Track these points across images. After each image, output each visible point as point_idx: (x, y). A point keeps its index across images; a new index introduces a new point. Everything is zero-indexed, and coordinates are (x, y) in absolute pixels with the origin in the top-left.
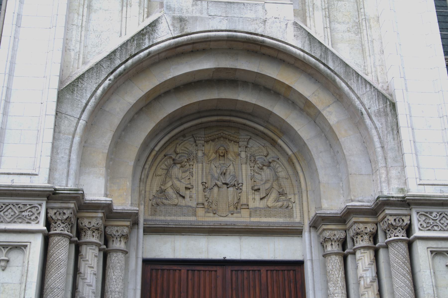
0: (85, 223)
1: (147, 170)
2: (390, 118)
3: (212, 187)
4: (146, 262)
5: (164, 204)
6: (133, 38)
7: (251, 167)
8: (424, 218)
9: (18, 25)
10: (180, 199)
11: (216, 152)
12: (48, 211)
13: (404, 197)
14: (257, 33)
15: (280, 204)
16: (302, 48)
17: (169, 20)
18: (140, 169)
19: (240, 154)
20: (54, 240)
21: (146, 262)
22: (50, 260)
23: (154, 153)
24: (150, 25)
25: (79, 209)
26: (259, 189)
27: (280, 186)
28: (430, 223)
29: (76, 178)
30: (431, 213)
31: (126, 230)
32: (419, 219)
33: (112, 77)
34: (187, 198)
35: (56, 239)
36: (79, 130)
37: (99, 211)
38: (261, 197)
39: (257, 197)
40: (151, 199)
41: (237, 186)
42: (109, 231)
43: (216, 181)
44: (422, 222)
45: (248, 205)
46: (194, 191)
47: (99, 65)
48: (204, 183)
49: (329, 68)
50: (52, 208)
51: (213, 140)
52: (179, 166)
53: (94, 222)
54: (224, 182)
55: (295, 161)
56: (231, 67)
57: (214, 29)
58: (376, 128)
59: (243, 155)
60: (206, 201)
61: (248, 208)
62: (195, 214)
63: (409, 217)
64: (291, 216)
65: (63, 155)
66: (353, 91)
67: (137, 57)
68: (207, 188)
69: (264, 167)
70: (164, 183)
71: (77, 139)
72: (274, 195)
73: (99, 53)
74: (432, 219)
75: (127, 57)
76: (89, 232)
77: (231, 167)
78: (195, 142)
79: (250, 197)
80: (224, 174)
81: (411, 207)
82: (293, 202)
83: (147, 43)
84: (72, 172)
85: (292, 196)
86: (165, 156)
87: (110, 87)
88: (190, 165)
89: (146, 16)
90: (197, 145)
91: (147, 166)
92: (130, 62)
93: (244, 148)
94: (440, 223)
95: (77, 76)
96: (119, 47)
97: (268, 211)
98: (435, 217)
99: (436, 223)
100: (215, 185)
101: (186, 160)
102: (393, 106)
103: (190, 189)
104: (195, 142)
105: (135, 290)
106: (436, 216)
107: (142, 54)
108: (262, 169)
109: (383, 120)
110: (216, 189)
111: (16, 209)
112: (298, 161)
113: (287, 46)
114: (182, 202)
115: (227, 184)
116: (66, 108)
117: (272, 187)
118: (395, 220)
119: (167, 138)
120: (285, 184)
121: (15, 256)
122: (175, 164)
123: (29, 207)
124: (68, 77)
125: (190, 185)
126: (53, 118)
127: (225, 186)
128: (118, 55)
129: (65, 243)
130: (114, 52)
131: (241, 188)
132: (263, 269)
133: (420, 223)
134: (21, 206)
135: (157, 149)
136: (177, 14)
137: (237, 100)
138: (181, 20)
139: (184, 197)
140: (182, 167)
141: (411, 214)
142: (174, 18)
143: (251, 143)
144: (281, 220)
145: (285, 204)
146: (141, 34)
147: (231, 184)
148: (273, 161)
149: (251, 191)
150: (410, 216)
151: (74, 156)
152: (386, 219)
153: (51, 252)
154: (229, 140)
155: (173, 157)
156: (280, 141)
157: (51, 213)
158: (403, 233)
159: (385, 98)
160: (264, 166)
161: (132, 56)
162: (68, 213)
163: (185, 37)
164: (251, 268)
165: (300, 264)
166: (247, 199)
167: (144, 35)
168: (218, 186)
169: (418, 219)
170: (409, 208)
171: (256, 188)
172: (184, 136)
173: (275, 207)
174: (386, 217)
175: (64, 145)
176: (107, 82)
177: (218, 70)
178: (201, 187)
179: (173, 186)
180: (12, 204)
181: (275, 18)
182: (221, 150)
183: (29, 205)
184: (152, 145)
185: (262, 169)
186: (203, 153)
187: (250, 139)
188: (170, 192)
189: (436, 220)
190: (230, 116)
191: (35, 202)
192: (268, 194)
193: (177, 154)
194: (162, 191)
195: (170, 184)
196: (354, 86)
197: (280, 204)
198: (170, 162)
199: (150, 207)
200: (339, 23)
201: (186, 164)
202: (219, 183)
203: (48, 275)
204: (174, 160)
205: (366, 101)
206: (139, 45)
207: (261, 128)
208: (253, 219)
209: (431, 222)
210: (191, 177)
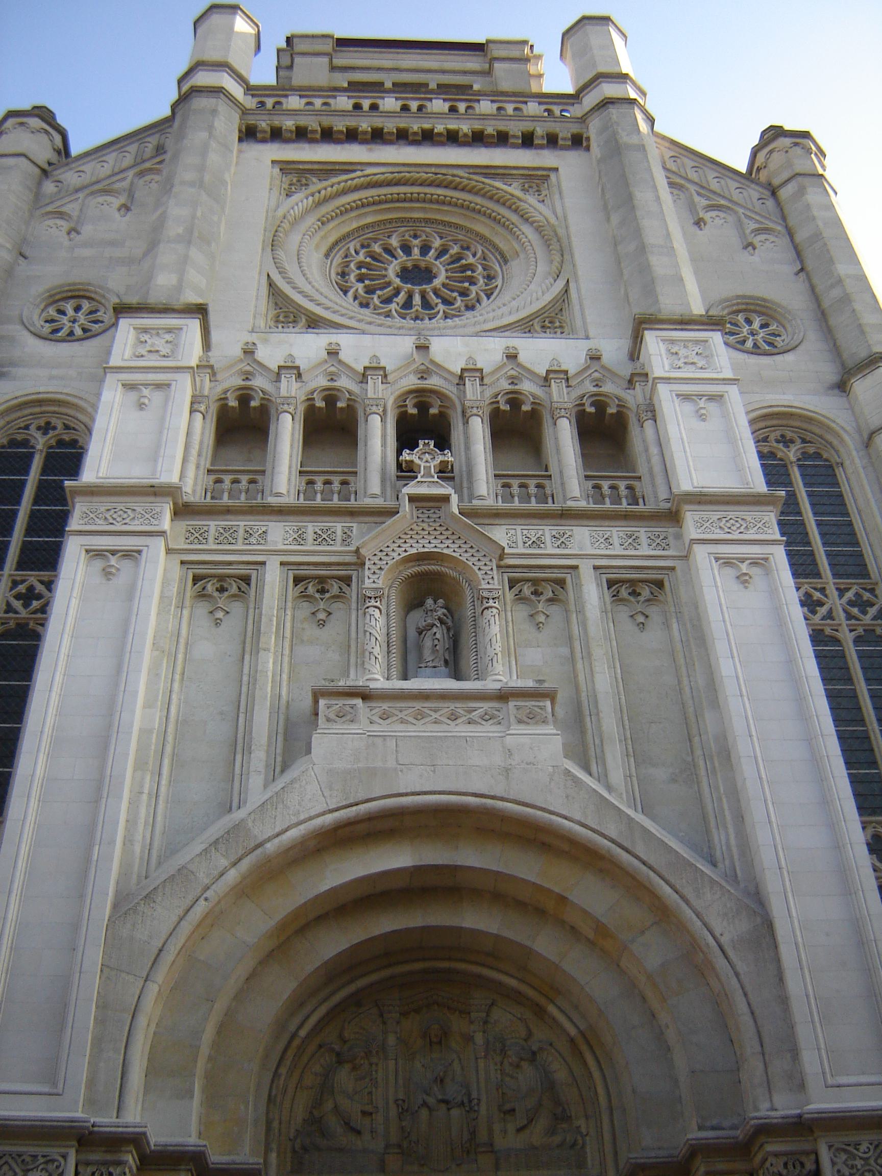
1: (283, 1078)
3: (417, 1108)
7: (496, 1064)
8: (844, 1156)
12: (80, 1169)
13: (800, 1116)
14: (492, 794)
15: (557, 1139)
16: (583, 820)
19: (473, 1036)
23: (296, 1042)
25: (141, 1164)
26: (513, 1110)
28: (856, 1166)
30: (857, 1145)
32: (835, 1159)
37: (183, 1167)
38: (518, 1127)
39: (511, 1128)
40: (292, 1138)
43: (425, 1097)
44: (840, 1166)
45: (491, 1145)
48: (400, 1102)
49: (637, 857)
50: (88, 1164)
51: (417, 1011)
52: (348, 1066)
54: (440, 1097)
55: (584, 1048)
56: (446, 863)
57: (409, 791)
58: (737, 975)
59: (479, 1038)
60: (406, 1138)
61: (492, 1152)
63: (813, 1157)
66: (687, 902)
68: (407, 1111)
69: (523, 1063)
72: (542, 1123)
74: (861, 1158)
75: (240, 852)
78: (382, 1015)
79: (497, 1127)
80: (442, 1081)
81: (815, 1135)
82: (585, 1133)
85: (582, 1123)
86: (320, 1046)
88: (371, 1064)
89: (278, 769)
90: (384, 1023)
91: (283, 1071)
93: (481, 1024)
94: (878, 1164)
96: (225, 833)
98: (865, 1153)
99: (870, 1165)
100: (422, 1105)
101: (362, 1054)
103: (371, 1114)
104: (382, 1015)
106: (867, 1150)
108: (518, 1066)
110: (424, 1112)
111: (18, 1165)
112: (591, 1048)
113: (554, 817)
115: (446, 1102)
118: (786, 1165)
119: (323, 1010)
122: (340, 1062)
123: (41, 1160)
124: (127, 895)
125: (370, 1106)
127: (443, 1107)
128: (223, 849)
131: (476, 1108)
133: (836, 1169)
134: (28, 1159)
135: (303, 1033)
137: (461, 928)
139: (359, 1132)
140: (354, 1068)
141: (817, 1150)
145: (568, 1139)
147: (456, 1101)
148: (541, 1049)
150: (816, 1154)
152: (768, 1164)
154: (449, 1008)
155: (337, 1048)
156: (551, 1009)
160: (522, 1059)
166: (490, 1131)
168: (428, 1107)
169: (832, 1160)
170: (811, 1138)
171: (507, 1107)
174: (766, 1159)
177: (417, 870)
178: (393, 1112)
180: (10, 1155)
181: (527, 764)
183: (43, 1156)
185: (518, 1066)
186: (398, 1038)
187: (492, 1004)
188: (333, 1122)
189: (868, 1159)
190: (449, 959)
191: (54, 1152)
192: (532, 1120)
193: (345, 1042)
195: (329, 1105)
197: (557, 1139)
199: (289, 1155)
201: (362, 1062)
202: (431, 1101)
204: (338, 1054)
207: (513, 983)
209: (859, 1163)
210: (374, 1089)
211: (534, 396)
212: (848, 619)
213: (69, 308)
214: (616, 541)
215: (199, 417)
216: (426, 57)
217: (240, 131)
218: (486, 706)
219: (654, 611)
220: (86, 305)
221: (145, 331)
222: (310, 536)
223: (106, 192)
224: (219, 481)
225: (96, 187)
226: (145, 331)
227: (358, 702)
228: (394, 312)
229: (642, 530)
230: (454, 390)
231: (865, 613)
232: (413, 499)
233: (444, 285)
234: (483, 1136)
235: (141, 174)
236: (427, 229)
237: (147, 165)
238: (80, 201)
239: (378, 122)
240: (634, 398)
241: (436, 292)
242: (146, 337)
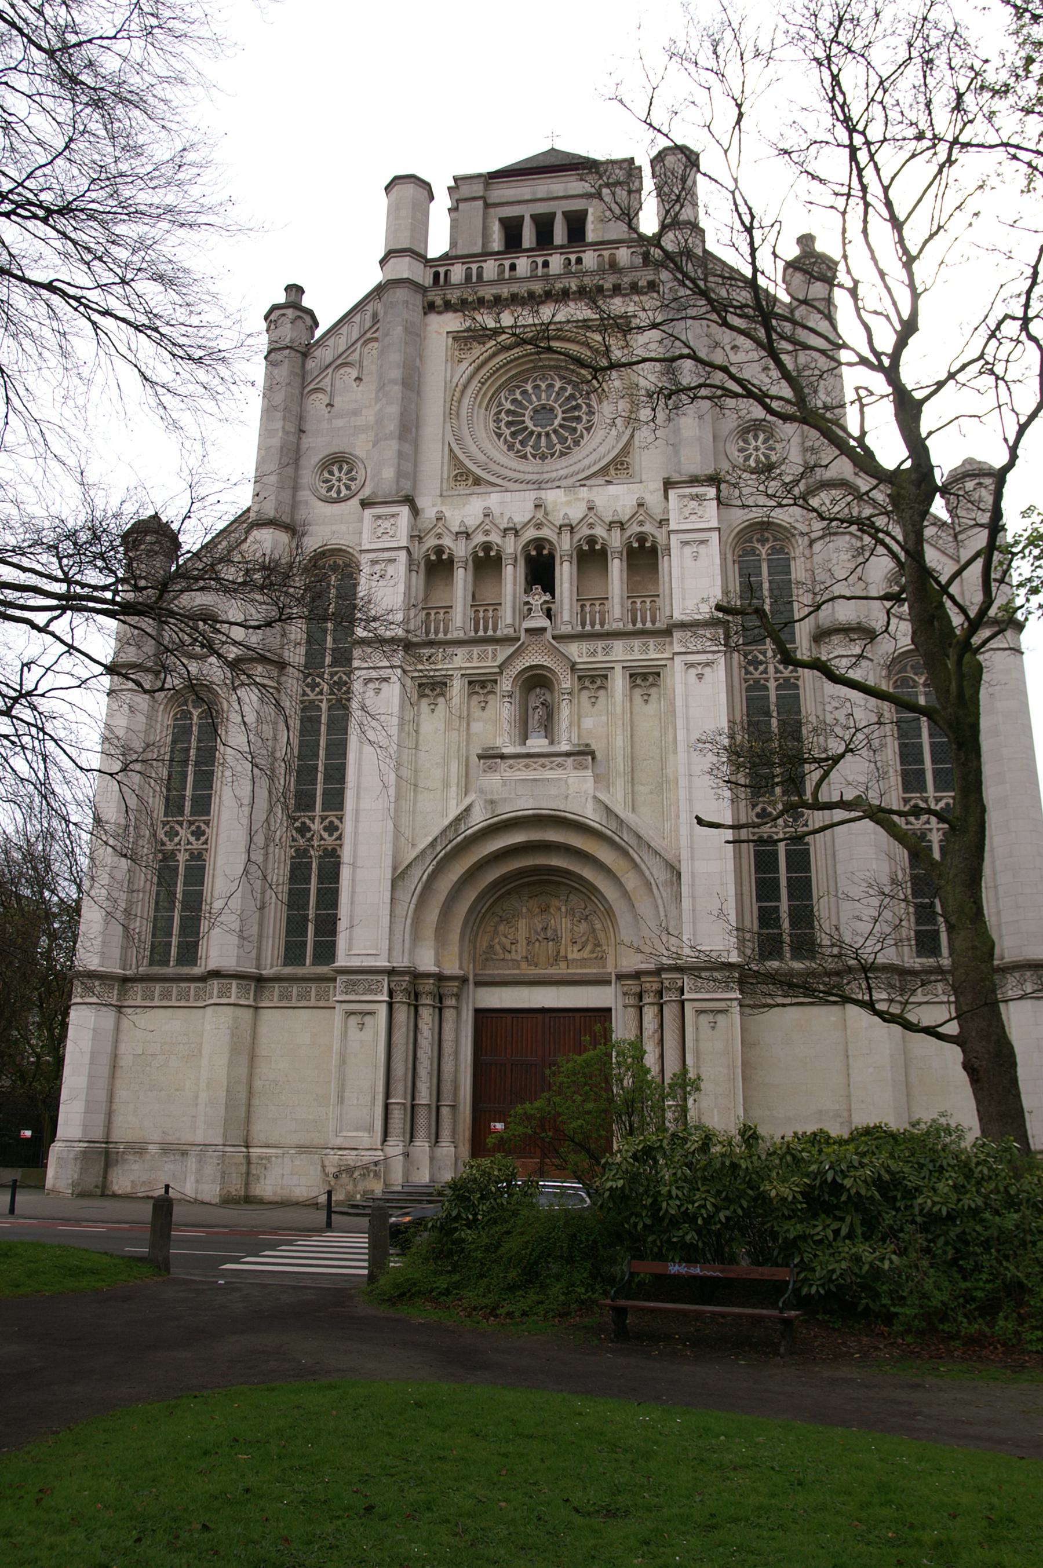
0: (421, 988)
2: (675, 888)
4: (478, 1012)
5: (493, 960)
6: (451, 824)
9: (357, 820)
10: (507, 954)
11: (539, 907)
15: (595, 955)
17: (481, 803)
18: (469, 930)
20: (396, 1006)
21: (478, 1012)
22: (394, 1022)
24: (465, 810)
27: (596, 938)
29: (410, 954)
31: (455, 990)
33: (434, 863)
34: (513, 953)
35: (398, 1005)
36: (410, 914)
39: (575, 949)
41: (556, 939)
42: (442, 991)
46: (519, 945)
47: (423, 852)
53: (427, 988)
59: (563, 909)
62: (519, 968)
64: (604, 967)
65: (398, 936)
67: (455, 842)
70: (492, 939)
71: (409, 921)
72: (589, 947)
73: (426, 836)
76: (424, 996)
77: (553, 921)
79: (569, 949)
83: (463, 827)
84: (406, 950)
87: (433, 871)
92: (449, 847)
95: (405, 865)
97: (583, 962)
102: (679, 874)
105: (466, 1037)
107: (459, 839)
109: (669, 890)
110: (537, 944)
114: (508, 956)
116: (399, 894)
117: (588, 940)
119: (491, 900)
120: (601, 935)
121: (368, 1019)
126: (389, 906)
129: (404, 1008)
130: (435, 839)
132: (578, 1015)
136: (489, 797)
138: (492, 802)
142: (486, 801)
143: (571, 897)
144: (595, 971)
146: (458, 819)
149: (570, 944)
151: (407, 937)
153: (394, 1016)
157: (392, 985)
158: (678, 993)
159: (672, 867)
161: (451, 842)
162: (404, 985)
163: (496, 819)
164: (566, 1015)
165: (609, 1010)
166: (566, 950)
167: (460, 820)
172: (509, 894)
173: (590, 959)
175: (399, 927)
176: (431, 867)
178: (525, 942)
179: (499, 943)
182: (543, 905)
184: (479, 908)
188: (498, 947)
191: (379, 978)
194: (492, 947)
195: (497, 940)
196: (645, 858)
197: (595, 955)
198: (497, 919)
200: (643, 785)
203: (393, 1034)
205: (655, 872)
206: (456, 830)
208: (569, 971)
211: (603, 539)
212: (776, 673)
213: (335, 469)
214: (636, 649)
215: (414, 574)
216: (554, 180)
217: (424, 308)
218: (560, 759)
219: (653, 691)
220: (345, 467)
221: (379, 517)
222: (475, 656)
223: (345, 364)
224: (428, 614)
225: (339, 362)
226: (379, 517)
227: (499, 760)
228: (529, 455)
229: (652, 640)
230: (556, 537)
231: (198, 839)
232: (527, 630)
233: (561, 426)
234: (562, 953)
235: (366, 343)
236: (551, 373)
237: (368, 335)
238: (330, 376)
239: (515, 288)
240: (660, 536)
241: (555, 431)
242: (380, 522)
